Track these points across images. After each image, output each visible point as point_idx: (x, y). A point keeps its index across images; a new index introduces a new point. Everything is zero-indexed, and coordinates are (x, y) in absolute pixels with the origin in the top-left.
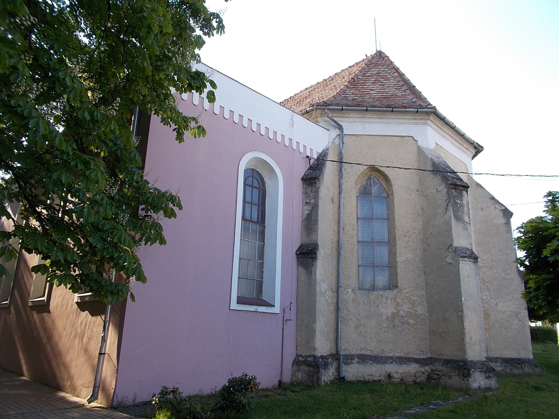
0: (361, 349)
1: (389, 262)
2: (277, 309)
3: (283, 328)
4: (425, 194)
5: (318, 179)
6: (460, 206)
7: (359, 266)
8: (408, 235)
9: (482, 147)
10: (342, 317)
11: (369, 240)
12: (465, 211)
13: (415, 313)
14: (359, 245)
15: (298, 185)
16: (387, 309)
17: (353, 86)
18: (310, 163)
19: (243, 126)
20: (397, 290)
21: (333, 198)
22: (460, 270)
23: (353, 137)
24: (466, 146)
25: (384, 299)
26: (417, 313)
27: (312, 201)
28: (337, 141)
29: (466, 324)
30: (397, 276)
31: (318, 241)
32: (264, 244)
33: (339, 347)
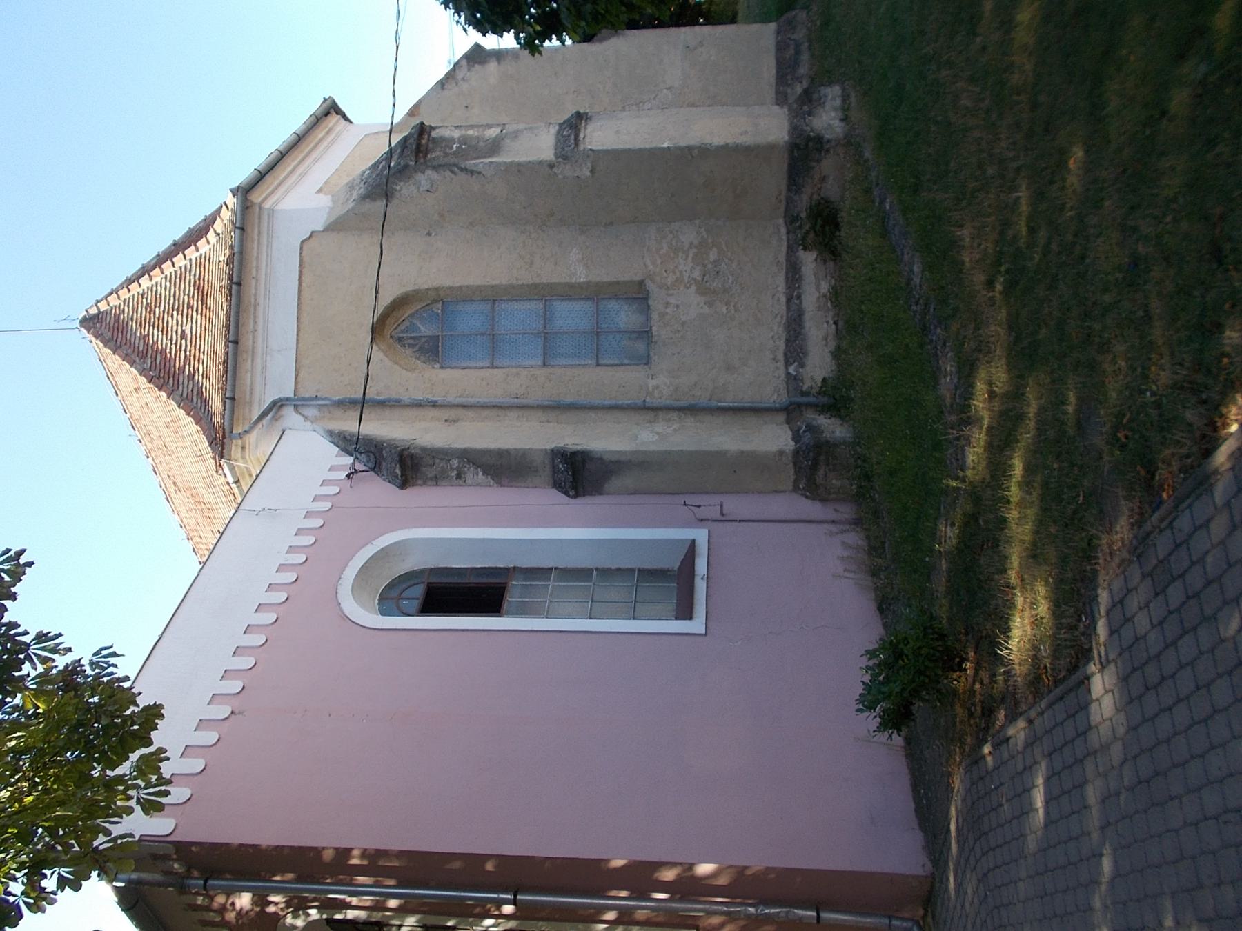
0: (775, 359)
1: (587, 299)
2: (700, 535)
3: (740, 521)
4: (436, 217)
5: (403, 450)
6: (465, 144)
7: (598, 365)
8: (529, 256)
9: (325, 100)
10: (710, 400)
11: (540, 342)
12: (476, 134)
13: (696, 247)
14: (552, 363)
15: (418, 496)
16: (691, 304)
17: (171, 379)
18: (364, 471)
19: (273, 624)
20: (648, 283)
21: (446, 421)
22: (605, 148)
23: (301, 375)
24: (323, 133)
25: (668, 310)
26: (696, 242)
27: (455, 463)
28: (311, 412)
29: (718, 141)
30: (618, 283)
31: (546, 449)
32: (556, 568)
33: (773, 405)
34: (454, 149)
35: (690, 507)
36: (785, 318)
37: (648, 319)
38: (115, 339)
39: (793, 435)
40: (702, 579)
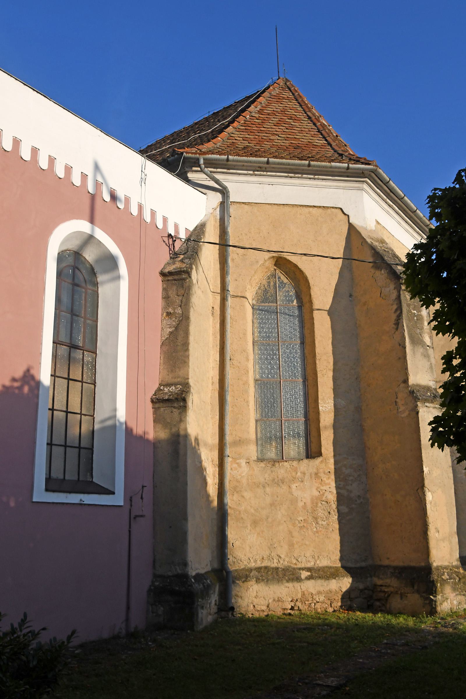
3: (130, 531)
6: (417, 319)
21: (213, 308)
27: (179, 311)
31: (188, 379)
34: (413, 312)
35: (142, 490)
36: (295, 566)
37: (293, 459)
38: (272, 97)
39: (201, 574)
40: (81, 500)
